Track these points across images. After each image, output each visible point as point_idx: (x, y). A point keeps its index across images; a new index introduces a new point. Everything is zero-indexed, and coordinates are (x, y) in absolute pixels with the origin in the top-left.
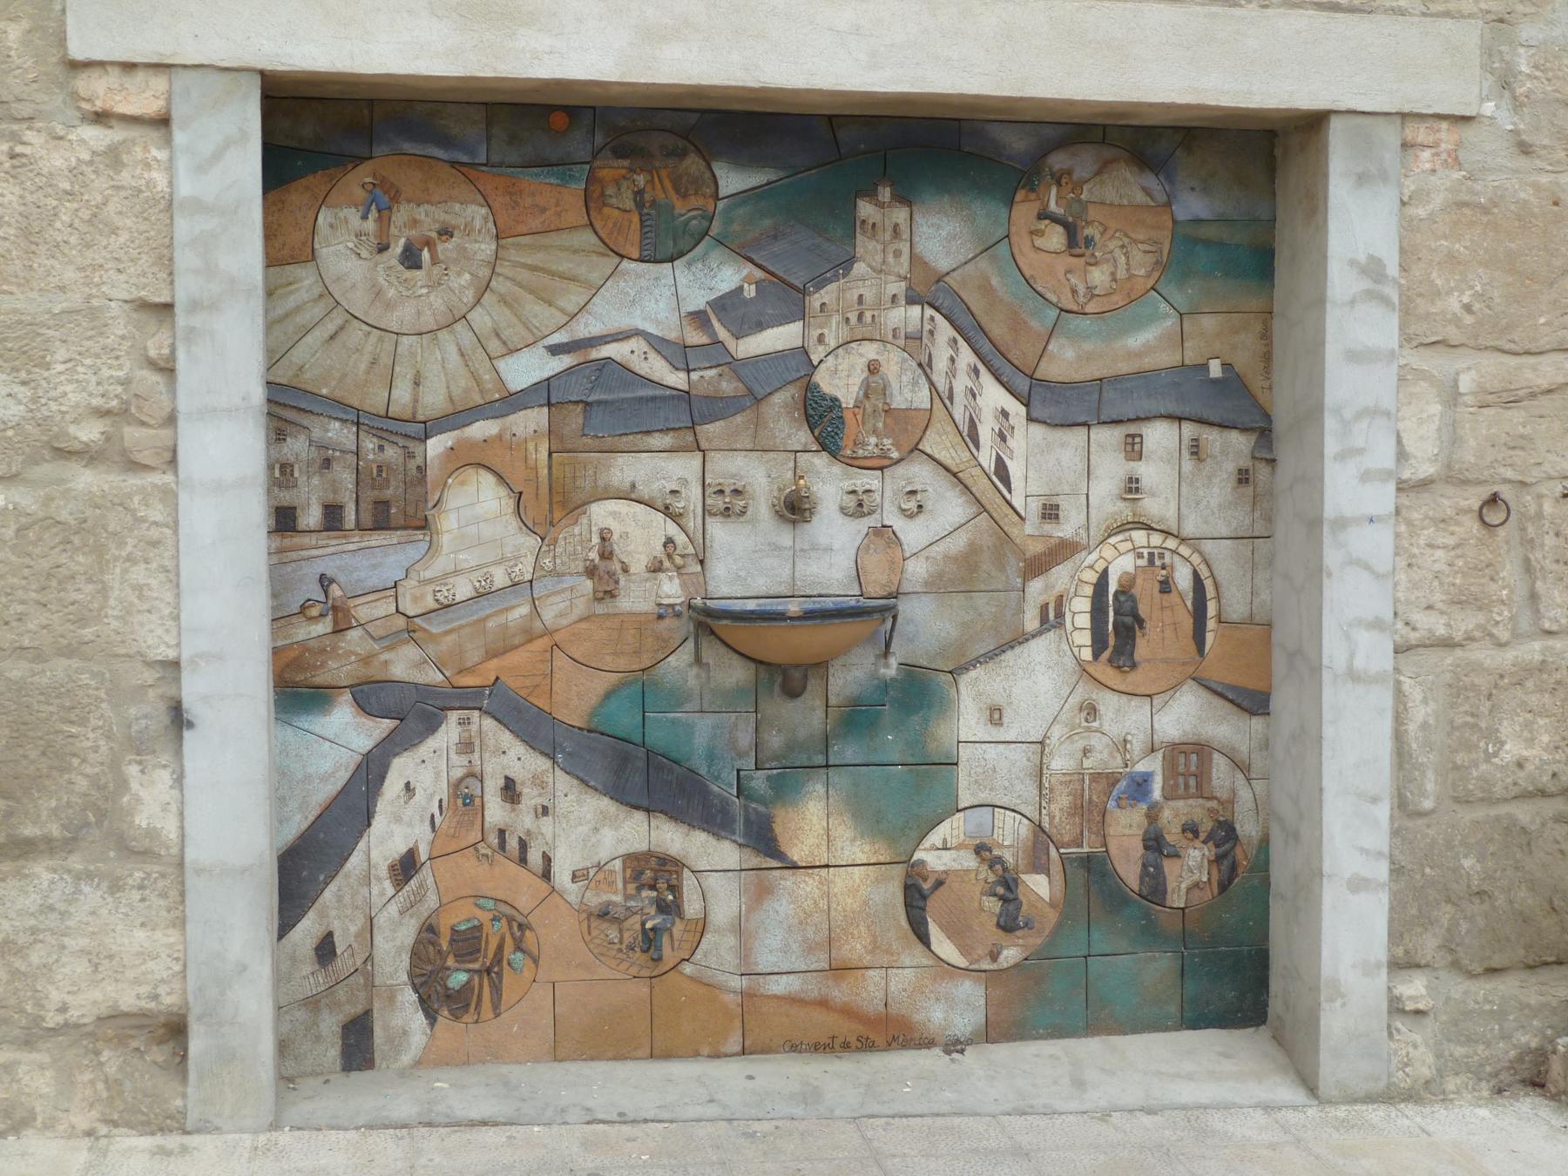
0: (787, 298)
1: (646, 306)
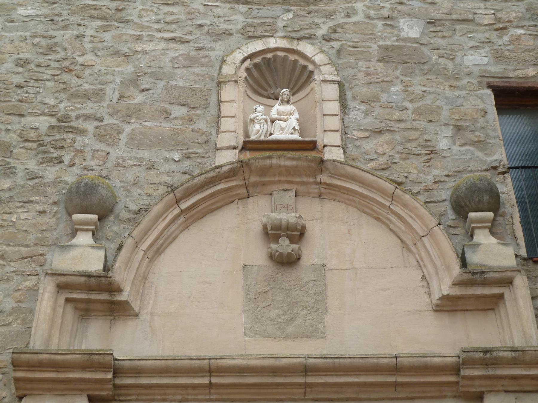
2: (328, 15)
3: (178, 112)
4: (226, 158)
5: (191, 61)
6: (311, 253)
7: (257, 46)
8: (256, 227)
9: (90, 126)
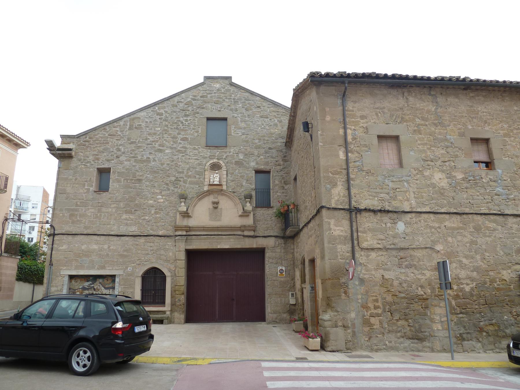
0: (93, 284)
1: (86, 284)
2: (226, 153)
3: (197, 176)
4: (206, 188)
5: (200, 164)
6: (220, 206)
7: (211, 162)
8: (211, 201)
9: (182, 179)
